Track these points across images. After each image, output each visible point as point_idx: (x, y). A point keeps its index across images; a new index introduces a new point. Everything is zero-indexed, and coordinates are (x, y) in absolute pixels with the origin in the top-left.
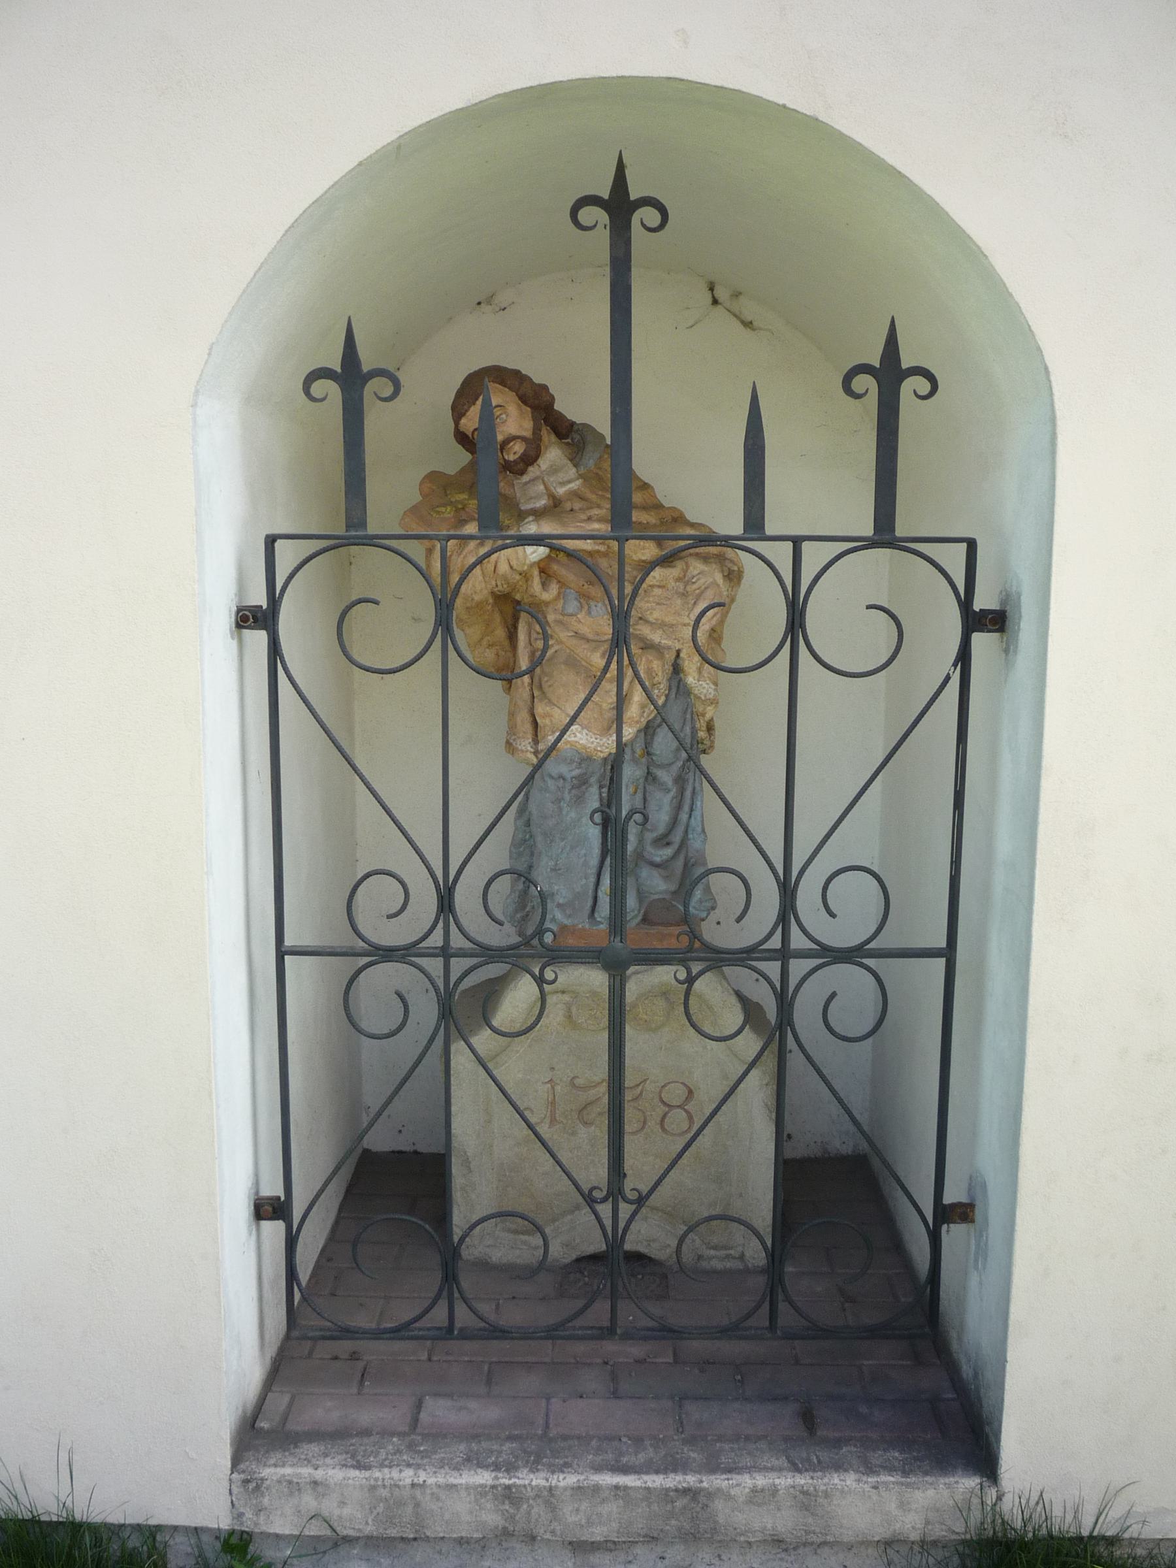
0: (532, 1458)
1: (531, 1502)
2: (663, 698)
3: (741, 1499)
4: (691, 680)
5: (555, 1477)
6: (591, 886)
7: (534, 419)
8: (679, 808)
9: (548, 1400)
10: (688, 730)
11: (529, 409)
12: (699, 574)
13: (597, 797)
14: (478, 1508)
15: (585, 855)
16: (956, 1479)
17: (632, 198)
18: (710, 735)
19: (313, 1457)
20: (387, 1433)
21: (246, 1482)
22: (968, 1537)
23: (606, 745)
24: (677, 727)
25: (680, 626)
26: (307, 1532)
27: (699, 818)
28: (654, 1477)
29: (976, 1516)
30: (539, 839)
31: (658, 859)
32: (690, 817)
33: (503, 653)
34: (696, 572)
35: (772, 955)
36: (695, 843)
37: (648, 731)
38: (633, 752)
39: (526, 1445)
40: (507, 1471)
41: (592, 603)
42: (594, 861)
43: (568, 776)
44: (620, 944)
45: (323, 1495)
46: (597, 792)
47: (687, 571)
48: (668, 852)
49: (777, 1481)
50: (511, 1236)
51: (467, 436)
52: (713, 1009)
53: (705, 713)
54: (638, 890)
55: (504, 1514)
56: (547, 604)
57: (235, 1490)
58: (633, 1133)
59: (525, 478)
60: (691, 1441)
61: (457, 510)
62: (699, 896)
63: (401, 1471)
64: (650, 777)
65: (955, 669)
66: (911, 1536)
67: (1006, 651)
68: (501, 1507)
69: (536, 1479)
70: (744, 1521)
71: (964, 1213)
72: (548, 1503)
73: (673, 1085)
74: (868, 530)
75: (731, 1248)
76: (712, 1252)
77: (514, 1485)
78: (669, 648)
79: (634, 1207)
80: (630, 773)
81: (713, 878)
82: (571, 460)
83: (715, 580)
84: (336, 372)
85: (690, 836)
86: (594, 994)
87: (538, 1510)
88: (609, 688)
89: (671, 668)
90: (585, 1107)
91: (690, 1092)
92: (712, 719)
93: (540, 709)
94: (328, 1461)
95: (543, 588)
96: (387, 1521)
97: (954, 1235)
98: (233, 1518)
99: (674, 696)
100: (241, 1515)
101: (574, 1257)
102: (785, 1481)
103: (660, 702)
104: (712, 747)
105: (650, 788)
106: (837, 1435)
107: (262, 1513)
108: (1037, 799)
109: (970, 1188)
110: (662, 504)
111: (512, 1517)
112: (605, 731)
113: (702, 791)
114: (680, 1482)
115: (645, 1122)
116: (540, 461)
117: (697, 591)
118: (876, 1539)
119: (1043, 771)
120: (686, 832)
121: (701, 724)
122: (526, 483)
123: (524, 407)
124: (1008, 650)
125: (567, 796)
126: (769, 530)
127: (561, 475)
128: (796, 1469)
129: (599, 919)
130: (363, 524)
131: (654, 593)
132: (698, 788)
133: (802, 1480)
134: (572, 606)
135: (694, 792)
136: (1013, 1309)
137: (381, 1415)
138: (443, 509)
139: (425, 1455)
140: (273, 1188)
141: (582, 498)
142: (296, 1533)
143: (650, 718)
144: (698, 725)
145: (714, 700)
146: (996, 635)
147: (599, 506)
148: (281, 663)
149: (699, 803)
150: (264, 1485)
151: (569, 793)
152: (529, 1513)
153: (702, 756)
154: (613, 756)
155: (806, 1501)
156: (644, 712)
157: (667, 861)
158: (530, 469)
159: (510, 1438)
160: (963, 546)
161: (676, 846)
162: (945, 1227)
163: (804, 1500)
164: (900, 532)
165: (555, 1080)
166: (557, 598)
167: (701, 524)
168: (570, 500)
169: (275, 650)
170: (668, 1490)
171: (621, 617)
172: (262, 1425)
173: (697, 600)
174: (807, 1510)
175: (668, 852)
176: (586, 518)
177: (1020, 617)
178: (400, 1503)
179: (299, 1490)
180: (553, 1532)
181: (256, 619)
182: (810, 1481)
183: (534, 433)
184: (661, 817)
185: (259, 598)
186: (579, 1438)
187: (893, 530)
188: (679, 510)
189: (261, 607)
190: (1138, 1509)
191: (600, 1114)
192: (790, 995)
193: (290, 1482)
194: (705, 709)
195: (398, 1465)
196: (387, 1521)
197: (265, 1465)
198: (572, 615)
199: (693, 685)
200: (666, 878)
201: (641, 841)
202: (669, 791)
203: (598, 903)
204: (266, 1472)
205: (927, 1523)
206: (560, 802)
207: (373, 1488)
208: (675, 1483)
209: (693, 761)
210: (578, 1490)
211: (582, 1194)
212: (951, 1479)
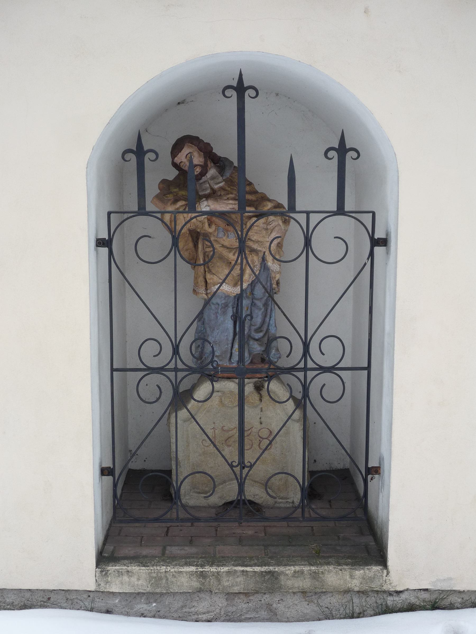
0: (210, 563)
1: (210, 577)
2: (258, 271)
3: (290, 575)
5: (220, 568)
6: (230, 348)
7: (205, 157)
8: (265, 316)
10: (269, 284)
11: (202, 153)
12: (272, 221)
14: (190, 580)
15: (227, 336)
16: (372, 567)
17: (245, 86)
19: (126, 563)
20: (154, 557)
23: (235, 290)
24: (264, 283)
25: (265, 242)
27: (274, 320)
28: (257, 568)
31: (257, 337)
32: (270, 320)
33: (192, 253)
34: (271, 220)
35: (300, 370)
37: (252, 285)
38: (246, 293)
39: (208, 559)
40: (201, 566)
41: (229, 233)
42: (231, 338)
43: (220, 304)
44: (242, 366)
45: (131, 576)
46: (232, 310)
47: (267, 220)
48: (261, 334)
49: (304, 568)
50: (197, 495)
52: (279, 398)
53: (276, 277)
54: (249, 350)
55: (200, 583)
56: (211, 233)
58: (247, 450)
59: (201, 181)
60: (271, 558)
61: (174, 196)
62: (274, 352)
63: (160, 567)
64: (253, 304)
65: (368, 260)
66: (355, 589)
69: (212, 569)
70: (291, 584)
72: (217, 578)
73: (264, 429)
75: (288, 499)
76: (280, 500)
77: (204, 571)
78: (260, 251)
80: (246, 302)
81: (279, 340)
82: (220, 173)
83: (279, 223)
84: (134, 150)
85: (270, 328)
86: (231, 392)
87: (213, 581)
88: (238, 268)
89: (262, 259)
92: (279, 280)
93: (208, 276)
94: (132, 565)
95: (210, 227)
96: (155, 586)
98: (97, 586)
99: (262, 270)
100: (99, 585)
102: (306, 569)
103: (257, 273)
104: (279, 291)
105: (253, 308)
107: (108, 584)
110: (257, 191)
111: (203, 583)
112: (235, 285)
113: (275, 309)
114: (267, 569)
115: (252, 445)
116: (207, 175)
117: (272, 228)
119: (397, 298)
121: (274, 282)
122: (202, 183)
123: (200, 153)
124: (388, 253)
125: (220, 311)
126: (297, 209)
128: (311, 565)
129: (233, 362)
130: (144, 208)
131: (254, 229)
132: (273, 308)
134: (221, 234)
135: (271, 310)
136: (391, 500)
137: (150, 551)
138: (169, 196)
140: (108, 464)
143: (253, 279)
144: (273, 282)
145: (280, 272)
146: (385, 247)
147: (232, 194)
148: (113, 258)
149: (273, 314)
150: (109, 573)
151: (221, 310)
152: (210, 582)
153: (275, 295)
154: (238, 296)
156: (250, 277)
157: (260, 338)
158: (203, 177)
159: (201, 558)
160: (371, 214)
161: (264, 332)
163: (314, 575)
164: (346, 209)
165: (215, 427)
166: (215, 231)
167: (274, 200)
168: (219, 190)
169: (111, 253)
170: (262, 572)
171: (242, 241)
172: (105, 555)
173: (272, 231)
175: (261, 334)
176: (226, 198)
177: (391, 241)
178: (161, 579)
179: (122, 574)
180: (219, 589)
181: (104, 244)
182: (316, 568)
184: (258, 320)
188: (264, 194)
189: (105, 239)
191: (234, 442)
192: (307, 385)
193: (118, 572)
194: (275, 276)
195: (159, 566)
196: (155, 586)
197: (108, 566)
199: (270, 266)
200: (260, 345)
201: (250, 330)
202: (261, 309)
203: (233, 355)
206: (217, 314)
208: (265, 569)
209: (271, 297)
210: (228, 573)
211: (229, 464)
212: (370, 567)
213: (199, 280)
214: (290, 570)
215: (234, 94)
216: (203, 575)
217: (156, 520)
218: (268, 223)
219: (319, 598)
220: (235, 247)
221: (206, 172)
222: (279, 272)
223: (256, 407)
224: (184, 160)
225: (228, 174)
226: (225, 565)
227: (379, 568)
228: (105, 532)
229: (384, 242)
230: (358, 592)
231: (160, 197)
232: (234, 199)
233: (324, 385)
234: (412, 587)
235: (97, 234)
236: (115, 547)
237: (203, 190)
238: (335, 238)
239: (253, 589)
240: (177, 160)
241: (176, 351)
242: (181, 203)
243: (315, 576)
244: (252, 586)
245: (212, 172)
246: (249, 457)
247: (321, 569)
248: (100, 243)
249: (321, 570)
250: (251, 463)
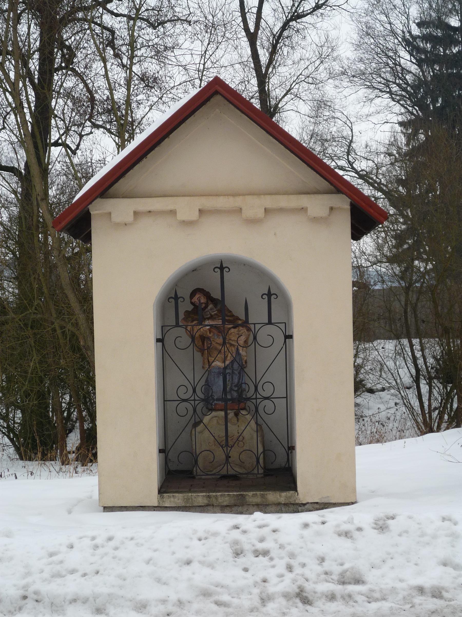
4: (241, 352)
35: (254, 399)
37: (232, 362)
87: (214, 500)
91: (244, 438)
93: (210, 358)
100: (160, 503)
102: (258, 493)
103: (234, 356)
104: (246, 366)
134: (216, 337)
169: (163, 345)
171: (224, 339)
178: (189, 499)
185: (160, 337)
210: (221, 495)
214: (251, 494)
215: (219, 270)
216: (209, 497)
218: (239, 331)
219: (266, 508)
221: (208, 306)
222: (246, 356)
223: (235, 425)
224: (196, 300)
225: (219, 307)
227: (293, 492)
230: (284, 504)
231: (185, 319)
232: (221, 319)
234: (310, 501)
237: (206, 315)
240: (193, 301)
241: (194, 391)
243: (263, 496)
244: (233, 502)
245: (211, 306)
247: (265, 493)
248: (158, 340)
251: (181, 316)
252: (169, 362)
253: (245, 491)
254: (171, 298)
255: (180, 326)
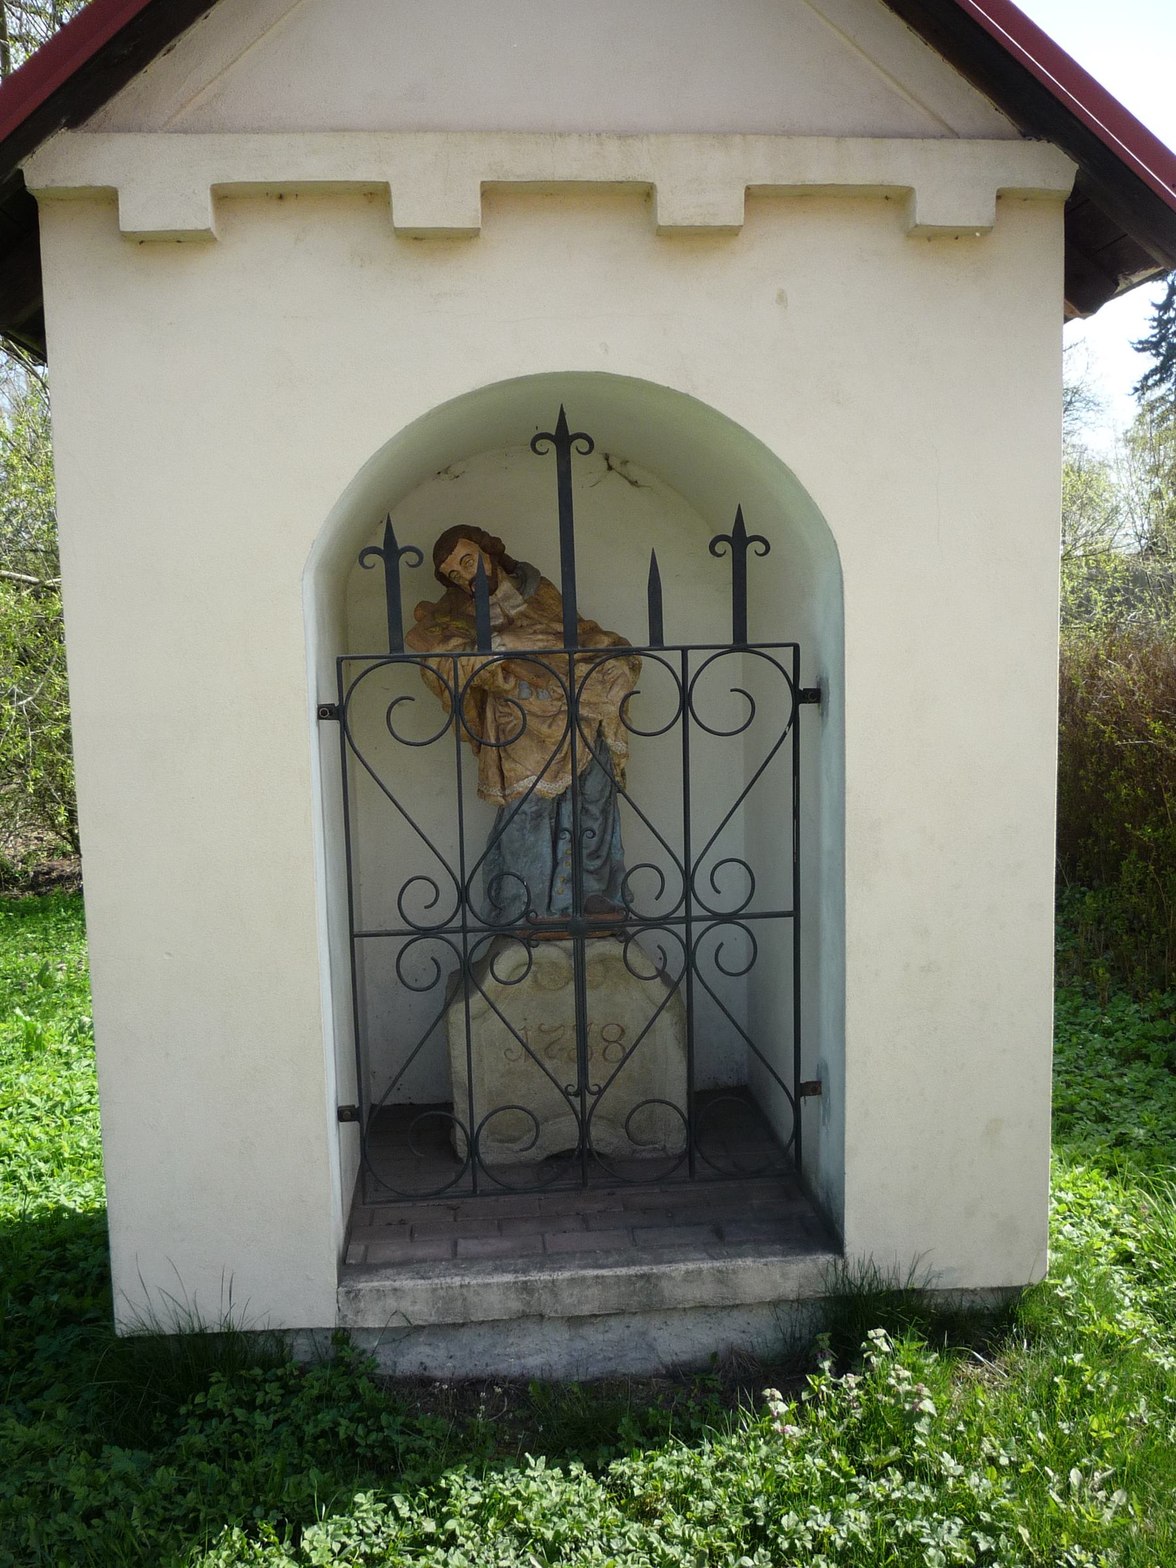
4: (610, 741)
6: (547, 889)
9: (543, 1235)
13: (548, 826)
18: (624, 779)
20: (437, 1260)
21: (348, 1293)
22: (828, 1294)
26: (390, 1325)
29: (831, 1279)
30: (508, 857)
34: (610, 667)
35: (678, 921)
36: (617, 857)
40: (524, 1273)
41: (539, 690)
48: (598, 863)
49: (701, 1266)
50: (499, 1144)
51: (444, 576)
57: (341, 1299)
67: (822, 714)
68: (521, 1297)
71: (815, 1088)
72: (552, 1291)
74: (729, 640)
77: (529, 1281)
78: (594, 719)
79: (595, 1097)
80: (567, 808)
82: (518, 589)
86: (554, 965)
87: (546, 1297)
90: (549, 1045)
91: (623, 1031)
93: (506, 766)
94: (401, 1277)
97: (808, 1104)
101: (545, 1155)
102: (706, 1265)
106: (738, 1239)
108: (844, 808)
109: (818, 1073)
111: (529, 1303)
116: (497, 592)
118: (768, 1300)
120: (610, 849)
121: (617, 772)
124: (823, 714)
125: (528, 826)
126: (666, 643)
127: (512, 601)
128: (712, 1258)
132: (617, 818)
133: (718, 1264)
134: (525, 693)
135: (614, 820)
139: (465, 1269)
141: (527, 617)
142: (383, 1326)
144: (615, 772)
155: (721, 1277)
159: (521, 1257)
161: (603, 859)
162: (802, 1099)
166: (515, 687)
167: (612, 633)
169: (344, 729)
170: (630, 1276)
174: (722, 1283)
175: (598, 863)
180: (556, 1311)
183: (492, 572)
186: (567, 1253)
187: (745, 640)
190: (935, 1268)
193: (378, 1291)
198: (525, 699)
200: (599, 880)
203: (553, 899)
204: (361, 1286)
205: (801, 1286)
207: (435, 1290)
210: (572, 1281)
213: (490, 774)
217: (437, 1194)
220: (551, 713)
225: (531, 591)
226: (564, 1267)
227: (829, 1257)
228: (346, 1221)
229: (815, 696)
233: (722, 944)
235: (318, 700)
236: (367, 1248)
238: (732, 690)
239: (615, 1307)
242: (455, 642)
245: (506, 587)
246: (596, 1078)
249: (731, 1267)
250: (599, 1087)
251: (408, 621)
252: (359, 774)
253: (658, 1261)
254: (374, 550)
255: (406, 659)
